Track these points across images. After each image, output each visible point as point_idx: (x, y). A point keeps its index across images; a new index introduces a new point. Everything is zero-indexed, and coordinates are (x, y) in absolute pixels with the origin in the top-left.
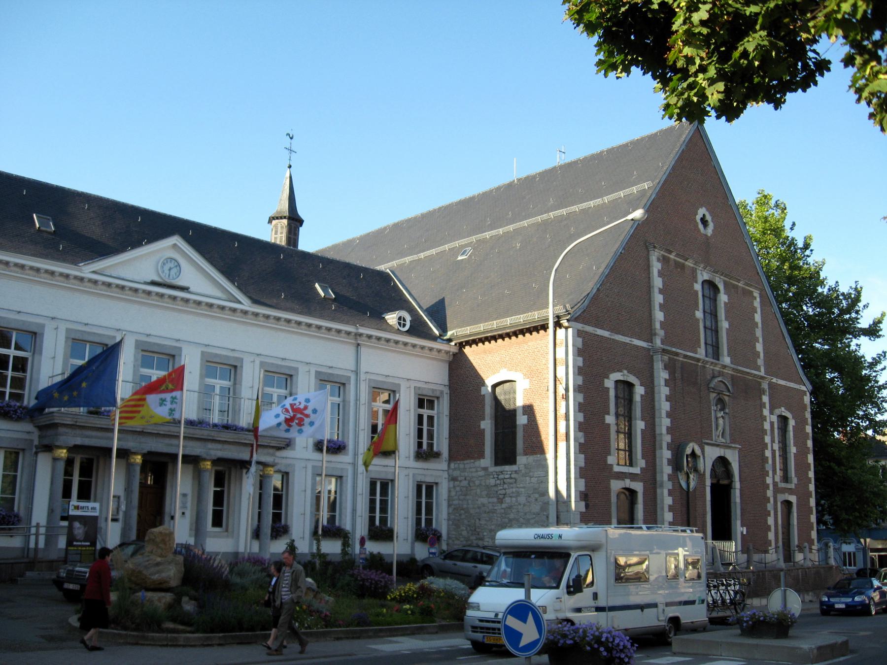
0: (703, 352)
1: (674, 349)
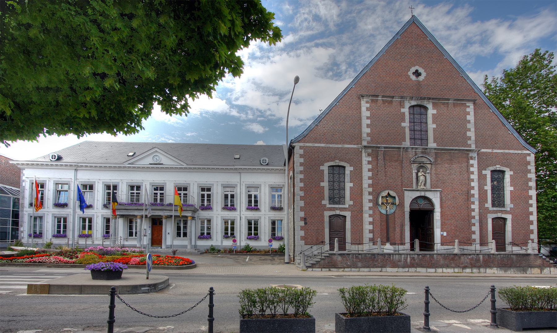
0: (409, 144)
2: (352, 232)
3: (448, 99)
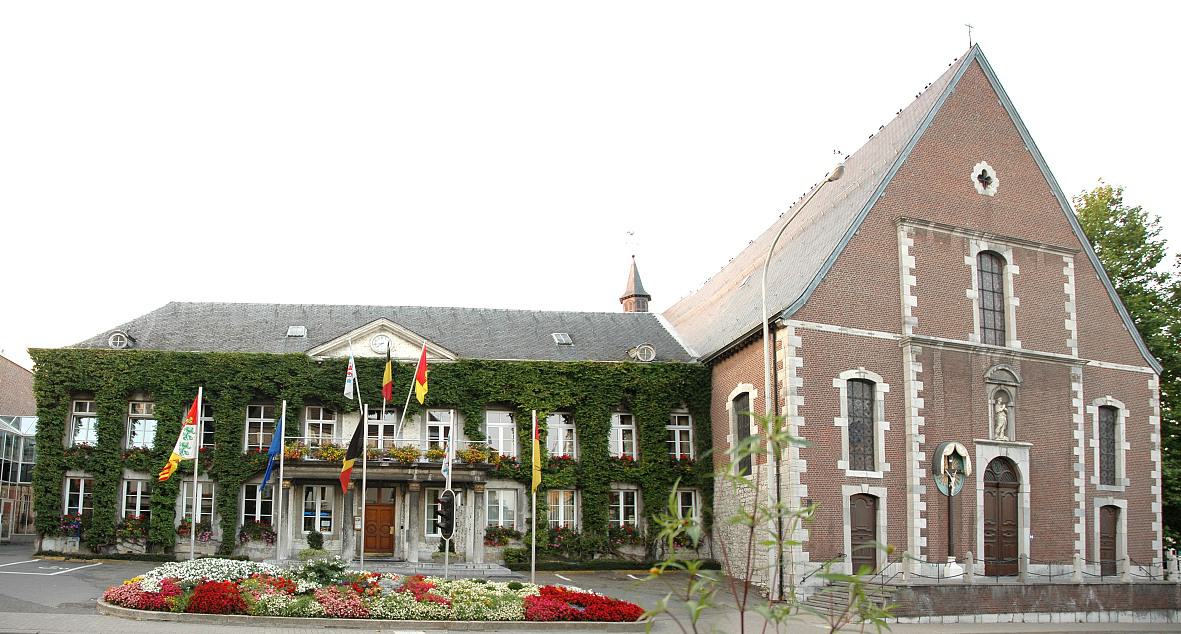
1: (932, 338)
3: (1037, 245)
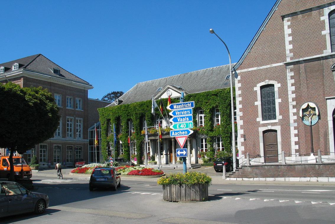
0: (330, 50)
2: (282, 145)
